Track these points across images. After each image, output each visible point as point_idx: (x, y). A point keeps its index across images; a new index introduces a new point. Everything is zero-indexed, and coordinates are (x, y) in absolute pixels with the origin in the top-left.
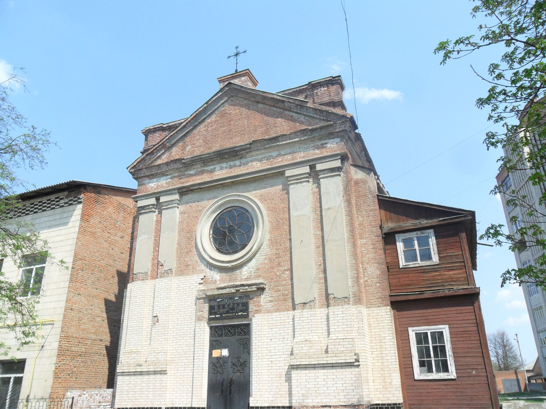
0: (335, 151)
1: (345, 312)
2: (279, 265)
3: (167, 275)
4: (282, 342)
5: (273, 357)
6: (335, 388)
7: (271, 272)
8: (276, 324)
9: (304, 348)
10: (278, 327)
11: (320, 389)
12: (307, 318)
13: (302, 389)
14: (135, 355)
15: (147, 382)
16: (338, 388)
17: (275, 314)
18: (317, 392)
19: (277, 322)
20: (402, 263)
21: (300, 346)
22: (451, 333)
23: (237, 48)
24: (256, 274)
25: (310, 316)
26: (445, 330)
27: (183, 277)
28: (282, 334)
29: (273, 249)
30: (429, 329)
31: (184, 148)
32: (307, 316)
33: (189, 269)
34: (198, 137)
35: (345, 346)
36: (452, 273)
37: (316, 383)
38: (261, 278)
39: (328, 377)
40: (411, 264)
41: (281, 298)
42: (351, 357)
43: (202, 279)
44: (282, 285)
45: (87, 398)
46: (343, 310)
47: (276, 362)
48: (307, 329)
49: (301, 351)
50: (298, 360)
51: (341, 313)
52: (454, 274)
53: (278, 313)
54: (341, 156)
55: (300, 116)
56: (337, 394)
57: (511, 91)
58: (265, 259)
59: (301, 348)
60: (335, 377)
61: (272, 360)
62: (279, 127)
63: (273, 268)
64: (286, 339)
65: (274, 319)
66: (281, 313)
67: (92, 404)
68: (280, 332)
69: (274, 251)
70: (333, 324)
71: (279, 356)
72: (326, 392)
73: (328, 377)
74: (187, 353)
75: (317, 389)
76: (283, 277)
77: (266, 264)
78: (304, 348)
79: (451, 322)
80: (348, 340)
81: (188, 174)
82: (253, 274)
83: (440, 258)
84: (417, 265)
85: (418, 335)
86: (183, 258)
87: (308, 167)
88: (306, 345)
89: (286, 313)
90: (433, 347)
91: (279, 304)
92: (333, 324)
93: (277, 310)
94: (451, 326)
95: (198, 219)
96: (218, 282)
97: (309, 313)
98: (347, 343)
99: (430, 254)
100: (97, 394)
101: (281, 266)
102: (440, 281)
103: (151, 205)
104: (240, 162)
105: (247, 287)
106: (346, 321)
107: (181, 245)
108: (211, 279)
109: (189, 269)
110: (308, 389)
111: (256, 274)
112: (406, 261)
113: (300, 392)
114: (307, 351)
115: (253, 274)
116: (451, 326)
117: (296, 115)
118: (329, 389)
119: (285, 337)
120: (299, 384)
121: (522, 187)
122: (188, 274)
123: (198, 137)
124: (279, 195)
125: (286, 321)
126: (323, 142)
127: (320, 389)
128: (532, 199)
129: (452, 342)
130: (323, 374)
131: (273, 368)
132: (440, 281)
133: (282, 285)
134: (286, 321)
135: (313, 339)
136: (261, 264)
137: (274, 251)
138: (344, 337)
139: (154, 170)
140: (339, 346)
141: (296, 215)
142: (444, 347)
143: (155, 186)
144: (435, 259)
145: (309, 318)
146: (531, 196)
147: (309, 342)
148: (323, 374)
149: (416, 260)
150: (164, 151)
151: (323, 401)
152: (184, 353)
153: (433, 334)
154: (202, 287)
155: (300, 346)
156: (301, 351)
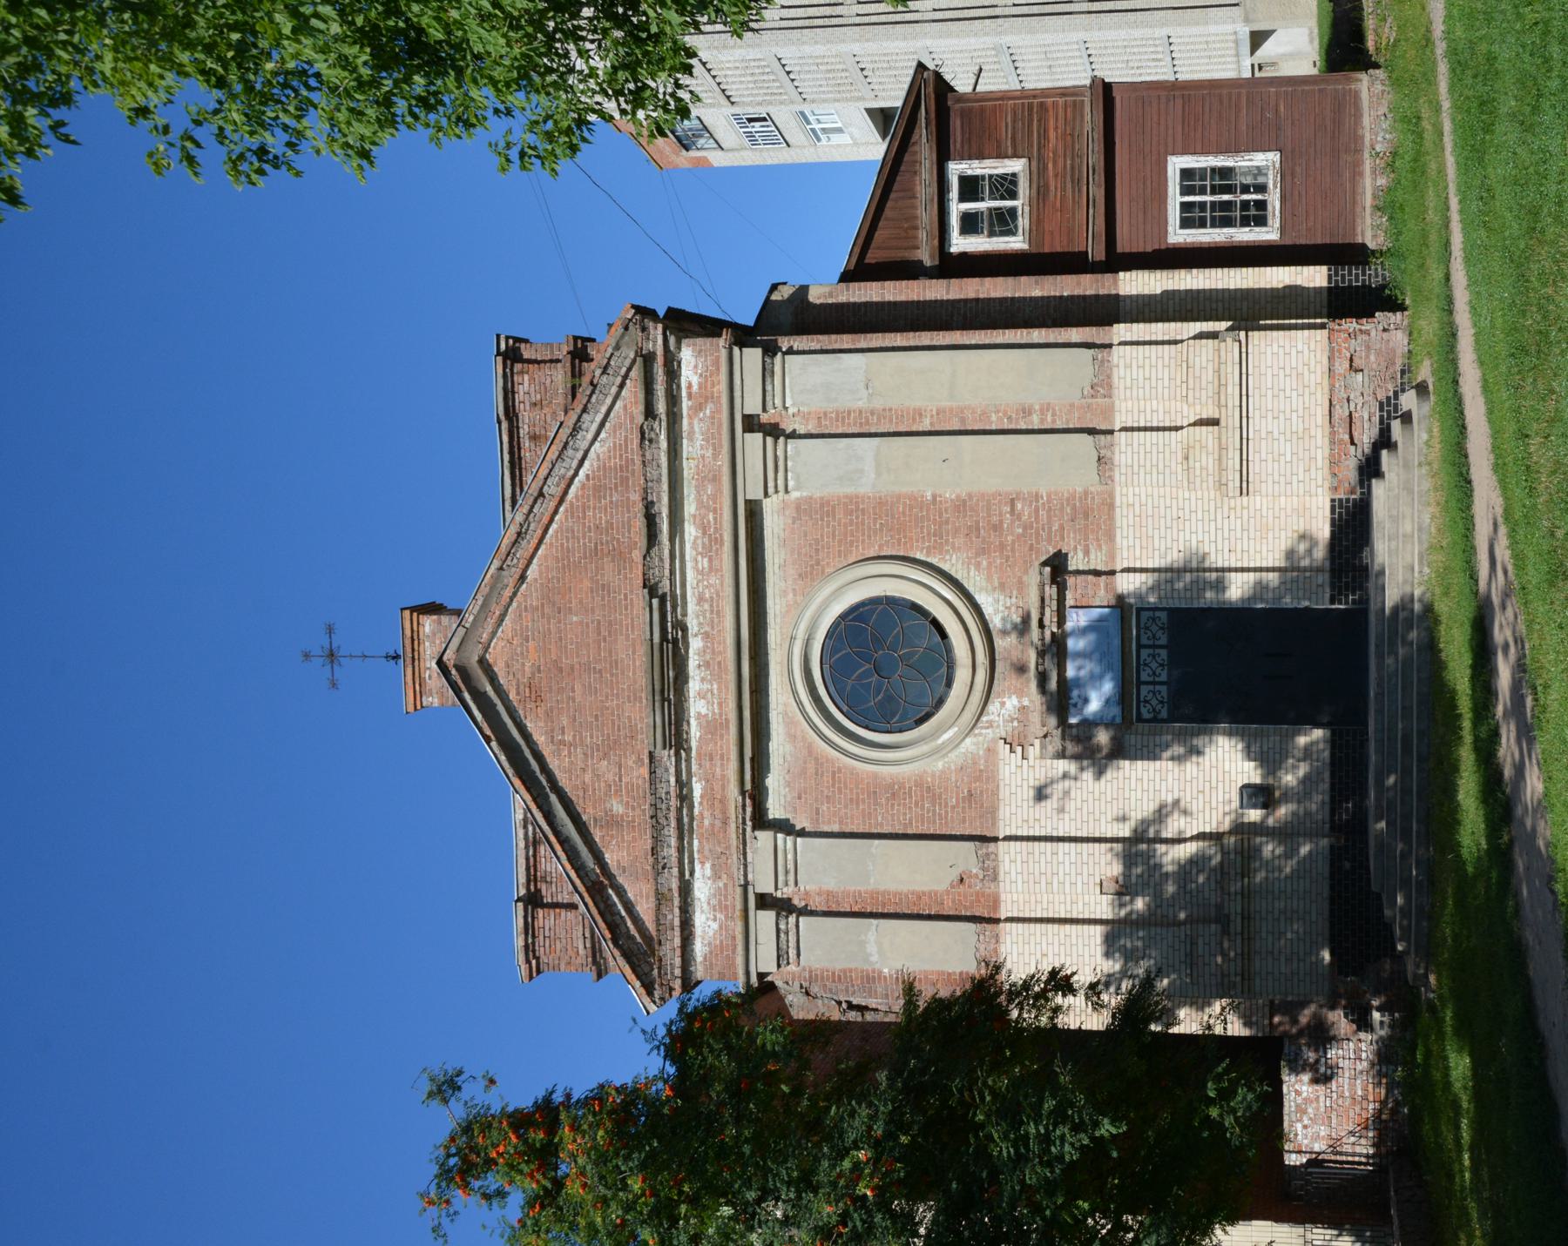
0: (716, 363)
1: (1128, 361)
2: (997, 528)
3: (993, 857)
4: (1187, 523)
5: (1220, 548)
6: (1294, 393)
7: (1013, 550)
8: (1144, 539)
9: (1204, 463)
10: (1150, 534)
11: (1294, 429)
12: (1136, 456)
13: (1295, 471)
14: (1200, 941)
15: (1270, 897)
16: (1294, 387)
17: (1118, 539)
18: (1301, 435)
19: (1138, 535)
20: (1016, 243)
21: (1198, 473)
22: (1184, 153)
23: (307, 656)
24: (1015, 593)
25: (1129, 448)
26: (1177, 164)
27: (1001, 808)
28: (1169, 525)
29: (953, 543)
30: (1175, 199)
31: (613, 822)
32: (1129, 454)
33: (981, 792)
34: (588, 777)
35: (1204, 365)
36: (1052, 134)
37: (1282, 437)
38: (1025, 578)
39: (1270, 407)
40: (1023, 222)
41: (1081, 522)
42: (1229, 349)
43: (1012, 751)
44: (1049, 522)
45: (1305, 1127)
46: (1008, 881)
47: (1233, 540)
48: (1161, 456)
49: (1211, 472)
50: (1230, 478)
51: (1128, 370)
52: (1056, 128)
53: (1118, 532)
54: (736, 344)
55: (592, 454)
56: (1307, 390)
57: (198, 145)
58: (978, 565)
59: (1204, 472)
60: (1270, 392)
61: (1226, 550)
62: (612, 518)
63: (1002, 547)
64: (1181, 514)
65: (1131, 544)
66: (1118, 524)
67: (1322, 1104)
68: (1163, 529)
69: (960, 541)
70: (1160, 355)
71: (1219, 532)
72: (1301, 414)
73: (1270, 407)
74: (1201, 789)
75: (1295, 436)
76: (1030, 517)
77: (990, 564)
78: (1204, 463)
79: (1162, 150)
80: (1191, 356)
81: (701, 803)
82: (1014, 600)
83: (1015, 155)
84: (1027, 209)
85: (1186, 223)
86: (946, 812)
87: (746, 435)
88: (1198, 459)
89: (1118, 511)
90: (1213, 192)
91: (1093, 531)
92: (1160, 355)
93: (1111, 536)
94: (1170, 149)
95: (840, 770)
96: (1026, 702)
97: (1123, 449)
98: (1197, 359)
99: (1003, 177)
100: (1296, 1091)
101: (1001, 522)
102: (1069, 162)
103: (777, 924)
104: (696, 635)
105: (1047, 611)
106: (1147, 361)
107: (911, 820)
108: (1015, 724)
109: (981, 792)
110: (1295, 457)
111: (1015, 593)
112: (1012, 233)
113: (1301, 478)
114: (1211, 458)
115: (1014, 600)
116: (1170, 149)
117: (587, 463)
118: (1294, 408)
119: (1175, 516)
120: (1282, 479)
121: (719, 84)
122: (995, 793)
123: (588, 777)
124: (810, 523)
125: (1137, 513)
126: (684, 393)
127: (1294, 429)
128: (763, 63)
129: (1205, 152)
130: (1263, 420)
131: (1245, 548)
132: (1069, 162)
133: (1049, 522)
134: (1137, 513)
135: (1185, 441)
136: (989, 578)
137: (960, 541)
138: (1184, 365)
139: (669, 917)
140: (1204, 378)
141: (873, 476)
142: (1213, 170)
143: (718, 916)
144: (1016, 166)
145: (1136, 450)
146: (752, 64)
147: (1191, 451)
148: (1263, 420)
149: (1012, 212)
150: (610, 891)
151: (1319, 422)
152: (1201, 796)
153: (1186, 191)
154: (1034, 751)
155: (1198, 473)
156: (1211, 472)
